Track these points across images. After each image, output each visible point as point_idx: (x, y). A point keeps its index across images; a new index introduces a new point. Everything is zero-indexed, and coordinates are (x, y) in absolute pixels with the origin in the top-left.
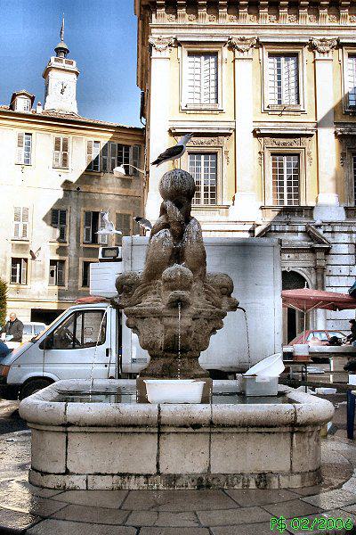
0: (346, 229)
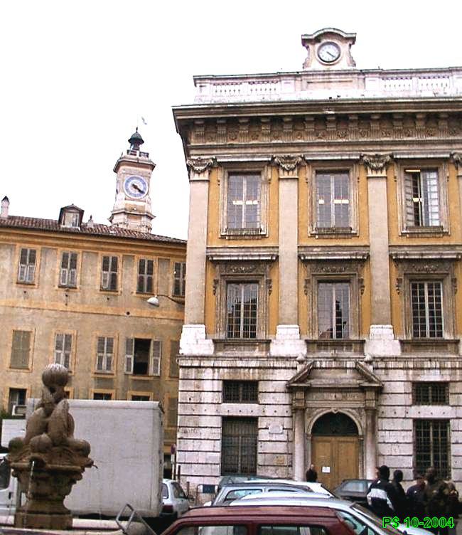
0: (401, 365)
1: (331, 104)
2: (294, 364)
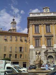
1: (47, 17)
2: (45, 49)
